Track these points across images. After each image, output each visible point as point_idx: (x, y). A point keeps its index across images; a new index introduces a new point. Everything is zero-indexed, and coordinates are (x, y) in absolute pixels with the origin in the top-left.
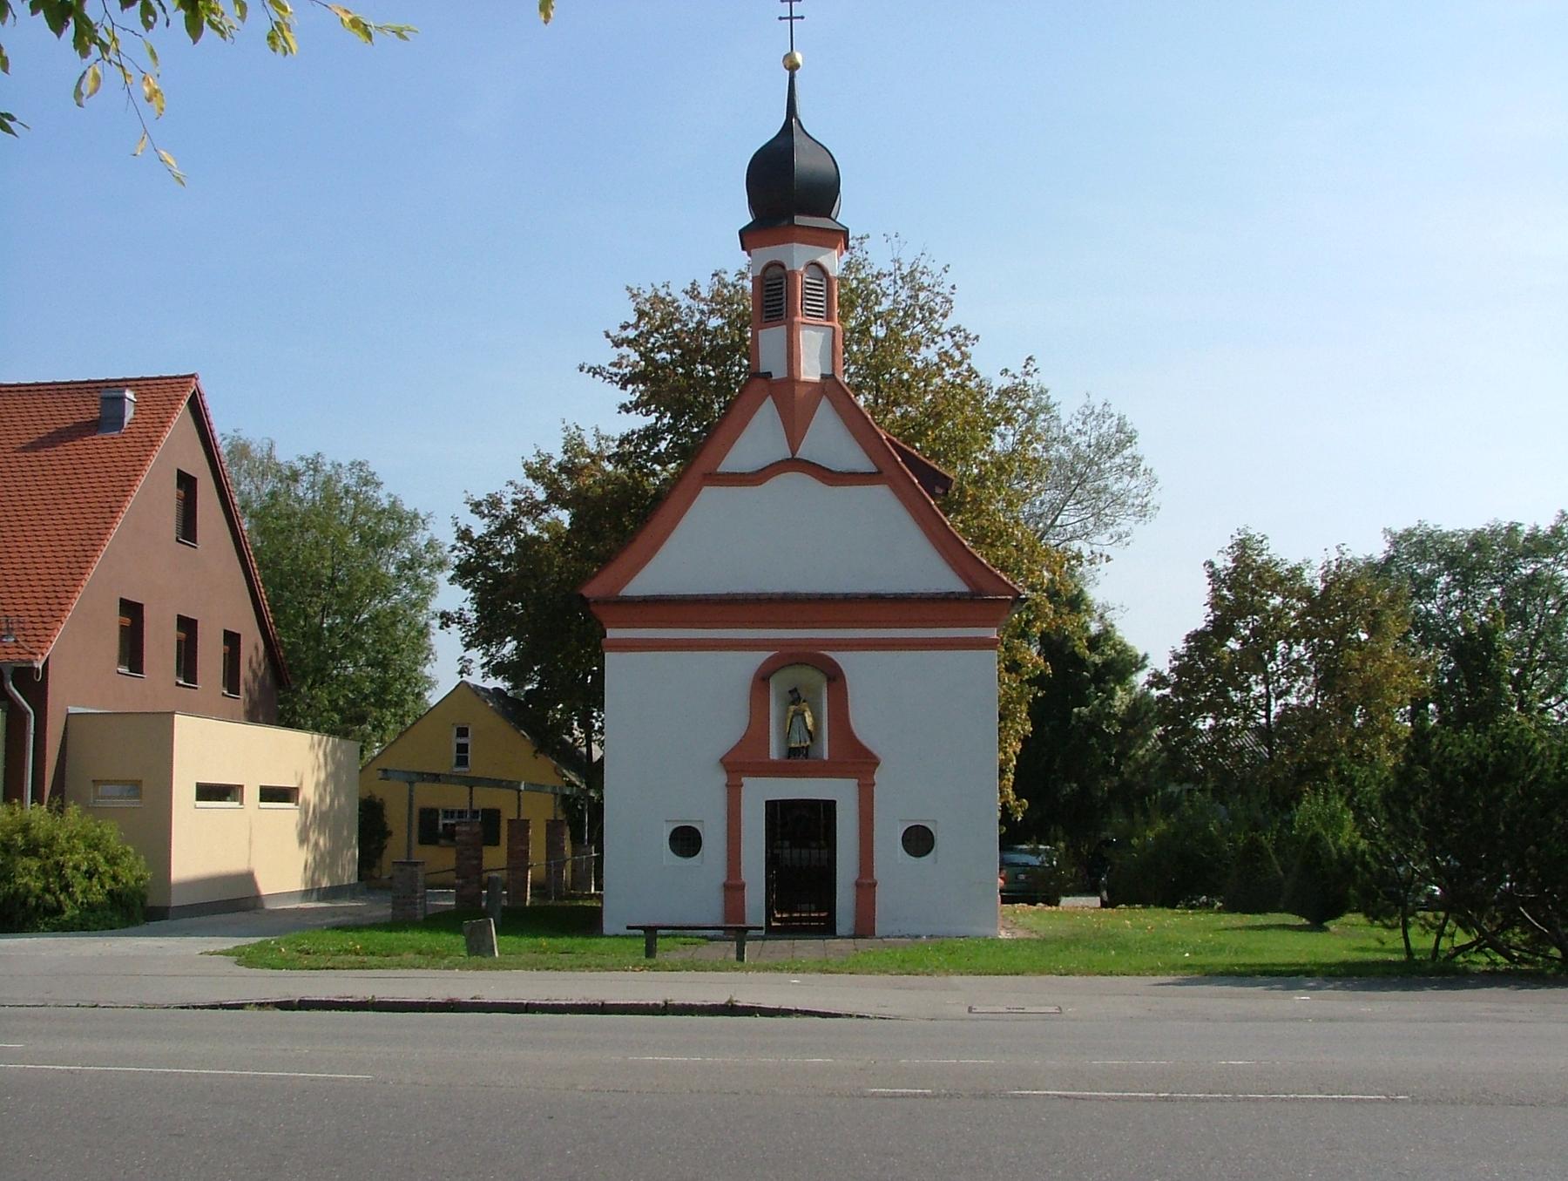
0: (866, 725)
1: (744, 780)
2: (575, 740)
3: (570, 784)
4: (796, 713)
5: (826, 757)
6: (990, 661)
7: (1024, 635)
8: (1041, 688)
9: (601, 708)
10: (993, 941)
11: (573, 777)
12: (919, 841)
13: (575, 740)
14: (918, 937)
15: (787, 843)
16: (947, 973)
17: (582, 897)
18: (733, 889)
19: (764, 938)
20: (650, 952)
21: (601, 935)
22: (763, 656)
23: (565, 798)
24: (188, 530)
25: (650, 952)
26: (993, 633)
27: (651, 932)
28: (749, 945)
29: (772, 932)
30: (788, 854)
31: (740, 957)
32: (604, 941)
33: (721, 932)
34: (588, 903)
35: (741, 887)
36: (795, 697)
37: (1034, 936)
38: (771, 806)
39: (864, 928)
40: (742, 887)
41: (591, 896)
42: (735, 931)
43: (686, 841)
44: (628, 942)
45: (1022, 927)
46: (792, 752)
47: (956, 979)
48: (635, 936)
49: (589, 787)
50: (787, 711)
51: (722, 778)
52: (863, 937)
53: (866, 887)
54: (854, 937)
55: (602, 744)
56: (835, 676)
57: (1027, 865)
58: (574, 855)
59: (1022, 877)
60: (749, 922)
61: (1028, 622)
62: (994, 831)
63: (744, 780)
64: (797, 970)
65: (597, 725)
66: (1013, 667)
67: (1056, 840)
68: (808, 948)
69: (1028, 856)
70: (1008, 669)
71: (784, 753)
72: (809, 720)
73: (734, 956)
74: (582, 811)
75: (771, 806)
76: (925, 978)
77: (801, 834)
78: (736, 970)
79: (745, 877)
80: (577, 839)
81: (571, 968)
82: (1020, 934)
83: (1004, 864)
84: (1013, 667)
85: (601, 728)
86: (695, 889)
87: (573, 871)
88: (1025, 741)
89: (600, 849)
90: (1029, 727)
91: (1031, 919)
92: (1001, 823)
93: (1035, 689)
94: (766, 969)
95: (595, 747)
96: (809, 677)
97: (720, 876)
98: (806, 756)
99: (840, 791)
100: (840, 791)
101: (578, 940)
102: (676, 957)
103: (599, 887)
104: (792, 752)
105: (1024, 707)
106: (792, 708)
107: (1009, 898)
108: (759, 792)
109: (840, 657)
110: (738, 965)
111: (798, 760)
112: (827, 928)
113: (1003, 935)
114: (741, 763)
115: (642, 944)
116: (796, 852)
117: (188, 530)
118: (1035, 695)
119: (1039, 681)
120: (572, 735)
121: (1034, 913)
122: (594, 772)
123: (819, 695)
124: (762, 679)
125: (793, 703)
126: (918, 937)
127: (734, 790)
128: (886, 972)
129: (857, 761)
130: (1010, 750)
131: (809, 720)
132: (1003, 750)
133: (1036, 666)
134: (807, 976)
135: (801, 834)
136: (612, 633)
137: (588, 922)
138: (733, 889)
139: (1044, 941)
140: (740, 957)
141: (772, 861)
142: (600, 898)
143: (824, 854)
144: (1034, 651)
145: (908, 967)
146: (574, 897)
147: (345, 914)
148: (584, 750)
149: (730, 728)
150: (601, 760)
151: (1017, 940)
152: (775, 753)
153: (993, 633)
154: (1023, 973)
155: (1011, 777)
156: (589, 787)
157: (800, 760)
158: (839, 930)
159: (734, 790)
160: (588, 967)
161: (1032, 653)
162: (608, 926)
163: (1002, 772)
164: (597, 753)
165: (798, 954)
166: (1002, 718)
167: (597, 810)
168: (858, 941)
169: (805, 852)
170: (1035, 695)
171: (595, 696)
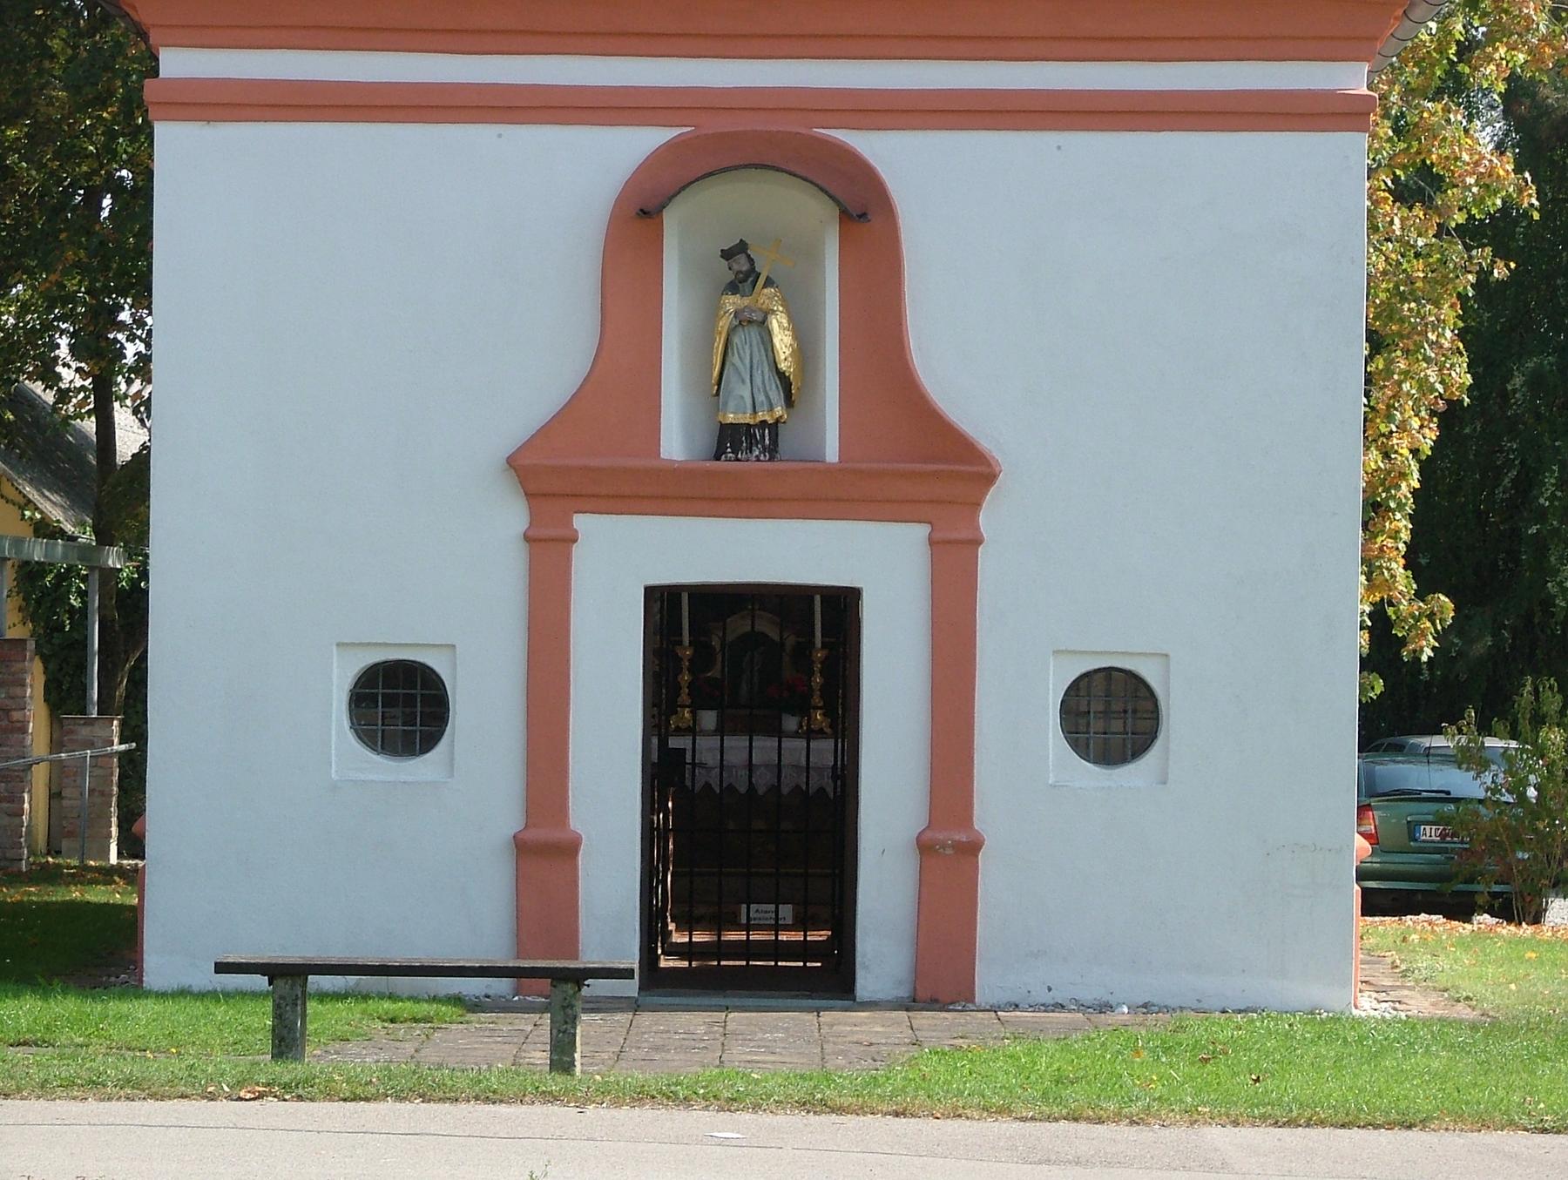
0: (953, 361)
1: (581, 522)
2: (63, 396)
3: (44, 529)
4: (743, 321)
5: (832, 453)
6: (1342, 165)
7: (1454, 87)
8: (1501, 253)
9: (142, 292)
10: (1332, 1027)
11: (53, 508)
12: (1112, 715)
13: (63, 396)
14: (1105, 1007)
15: (709, 719)
16: (1192, 1117)
17: (83, 876)
18: (544, 853)
19: (635, 1006)
20: (286, 1042)
21: (136, 989)
22: (642, 141)
23: (30, 573)
24: (221, 968)
25: (286, 1042)
26: (1352, 79)
27: (289, 978)
28: (588, 1026)
29: (657, 984)
30: (720, 752)
31: (562, 1057)
32: (141, 1011)
33: (502, 986)
34: (97, 895)
35: (568, 850)
36: (740, 269)
37: (1463, 1012)
38: (663, 603)
39: (941, 982)
40: (972, 848)
41: (107, 875)
42: (553, 984)
43: (401, 705)
44: (220, 1011)
45: (1429, 984)
46: (731, 439)
47: (1218, 1137)
48: (243, 994)
49: (105, 537)
50: (714, 312)
51: (510, 517)
52: (935, 1003)
53: (949, 853)
54: (913, 1003)
55: (142, 409)
56: (863, 209)
57: (1445, 797)
58: (56, 745)
59: (1429, 833)
60: (590, 957)
61: (1467, 49)
62: (1343, 690)
63: (581, 522)
64: (731, 1104)
65: (131, 350)
66: (1418, 186)
67: (1538, 720)
68: (772, 1035)
69: (1453, 769)
70: (1403, 195)
71: (707, 440)
72: (783, 341)
73: (540, 1056)
74: (80, 617)
75: (663, 603)
76: (1125, 1132)
77: (752, 692)
78: (551, 1098)
79: (581, 817)
80: (64, 697)
81: (44, 1089)
82: (1419, 1004)
83: (1371, 794)
84: (1418, 186)
85: (144, 360)
86: (423, 853)
87: (55, 796)
88: (1450, 417)
89: (136, 731)
90: (1462, 376)
91: (1453, 963)
92: (1366, 664)
93: (1483, 255)
94: (642, 1096)
95: (122, 416)
96: (789, 211)
97: (503, 813)
98: (773, 451)
99: (874, 561)
100: (874, 561)
101: (66, 1006)
102: (364, 1060)
103: (133, 845)
104: (731, 439)
105: (1449, 312)
106: (732, 302)
107: (1382, 900)
108: (627, 560)
109: (878, 148)
110: (556, 1083)
111: (746, 458)
112: (829, 977)
113: (1367, 1006)
114: (569, 474)
115: (261, 1017)
116: (736, 746)
117: (221, 968)
118: (1484, 276)
119: (1496, 230)
120: (49, 376)
121: (1462, 944)
122: (121, 498)
123: (813, 257)
124: (641, 212)
125: (733, 288)
126: (1105, 1007)
127: (548, 554)
128: (1004, 1111)
129: (931, 470)
130: (1402, 445)
131: (783, 341)
132: (1374, 439)
133: (1488, 184)
134: (765, 1119)
135: (752, 692)
136: (176, 63)
137: (96, 951)
138: (544, 853)
139: (1492, 1028)
140: (562, 1057)
141: (663, 773)
142: (134, 878)
143: (824, 750)
144: (1485, 135)
145: (1075, 1096)
146: (50, 876)
147: (1428, 752)
148: (89, 426)
149: (540, 360)
150: (142, 459)
151: (1410, 1024)
152: (676, 439)
153: (1352, 79)
154: (1424, 1124)
155: (1403, 525)
156: (105, 537)
157: (752, 464)
158: (866, 984)
159: (548, 554)
160: (94, 1086)
161: (1478, 148)
162: (161, 960)
163: (1375, 510)
164: (128, 437)
165: (738, 1053)
166: (1377, 343)
167: (129, 611)
168: (924, 1018)
169: (765, 747)
170: (1484, 276)
171: (124, 264)
